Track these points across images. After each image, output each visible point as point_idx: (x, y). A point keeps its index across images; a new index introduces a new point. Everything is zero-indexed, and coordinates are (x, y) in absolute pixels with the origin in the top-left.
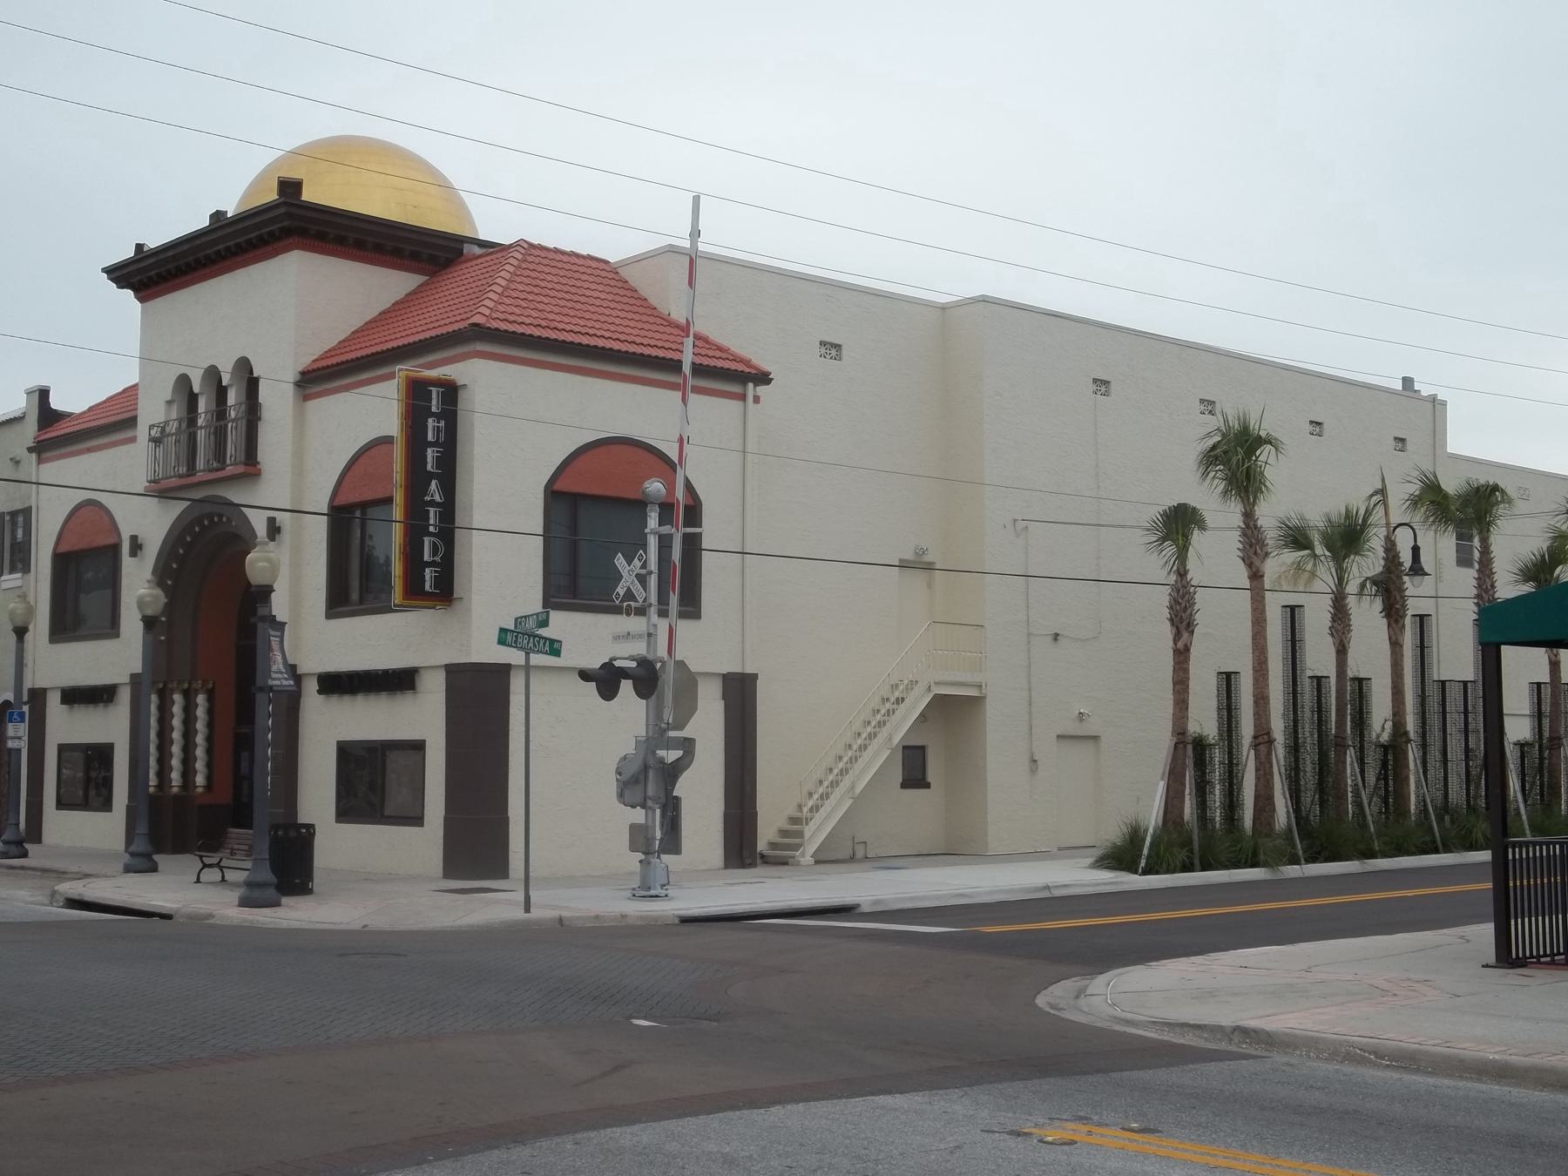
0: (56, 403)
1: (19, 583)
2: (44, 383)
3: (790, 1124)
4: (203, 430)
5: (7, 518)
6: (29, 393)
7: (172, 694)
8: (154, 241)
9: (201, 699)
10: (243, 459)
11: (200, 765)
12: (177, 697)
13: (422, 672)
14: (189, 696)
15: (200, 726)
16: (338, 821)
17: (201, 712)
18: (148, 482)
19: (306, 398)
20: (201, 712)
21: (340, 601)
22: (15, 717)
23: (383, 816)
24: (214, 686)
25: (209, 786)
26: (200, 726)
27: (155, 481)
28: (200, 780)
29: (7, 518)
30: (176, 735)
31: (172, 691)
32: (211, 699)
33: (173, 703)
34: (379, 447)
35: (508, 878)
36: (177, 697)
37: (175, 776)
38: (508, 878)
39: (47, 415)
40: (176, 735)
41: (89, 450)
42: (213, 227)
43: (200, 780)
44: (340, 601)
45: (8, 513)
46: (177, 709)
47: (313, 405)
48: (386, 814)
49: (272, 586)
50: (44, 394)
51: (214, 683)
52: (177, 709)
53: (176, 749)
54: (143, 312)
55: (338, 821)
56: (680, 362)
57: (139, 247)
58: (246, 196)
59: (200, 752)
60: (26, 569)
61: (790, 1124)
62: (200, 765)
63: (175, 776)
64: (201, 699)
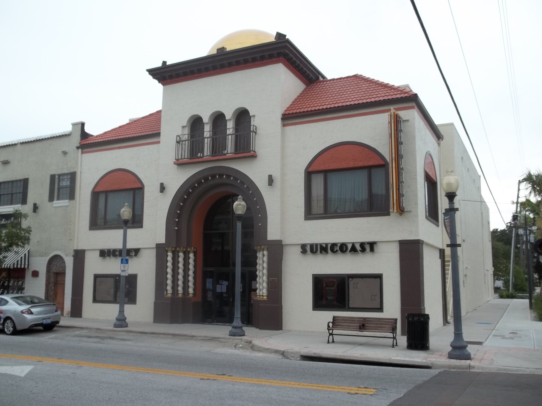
0: (87, 130)
1: (67, 204)
2: (83, 121)
3: (65, 388)
4: (187, 142)
5: (57, 177)
6: (74, 125)
7: (189, 254)
8: (170, 62)
9: (191, 255)
10: (234, 152)
11: (191, 284)
12: (181, 255)
13: (378, 243)
14: (186, 254)
15: (191, 267)
16: (314, 309)
17: (191, 261)
18: (176, 160)
19: (284, 125)
20: (191, 261)
21: (94, 225)
22: (124, 261)
23: (349, 308)
24: (196, 250)
25: (195, 294)
26: (191, 267)
27: (177, 160)
28: (191, 291)
29: (57, 177)
30: (181, 271)
31: (178, 252)
32: (195, 256)
33: (179, 257)
34: (343, 146)
35: (281, 329)
36: (181, 255)
37: (180, 289)
38: (281, 329)
39: (84, 135)
40: (181, 271)
41: (120, 148)
42: (163, 67)
43: (191, 291)
44: (94, 225)
45: (58, 175)
46: (181, 259)
47: (288, 128)
48: (350, 306)
49: (455, 193)
50: (83, 125)
51: (197, 249)
52: (181, 259)
53: (180, 277)
54: (164, 90)
55: (314, 309)
56: (237, 151)
57: (164, 63)
58: (210, 52)
59: (191, 278)
60: (72, 196)
61: (65, 388)
62: (191, 284)
63: (180, 289)
64: (191, 255)
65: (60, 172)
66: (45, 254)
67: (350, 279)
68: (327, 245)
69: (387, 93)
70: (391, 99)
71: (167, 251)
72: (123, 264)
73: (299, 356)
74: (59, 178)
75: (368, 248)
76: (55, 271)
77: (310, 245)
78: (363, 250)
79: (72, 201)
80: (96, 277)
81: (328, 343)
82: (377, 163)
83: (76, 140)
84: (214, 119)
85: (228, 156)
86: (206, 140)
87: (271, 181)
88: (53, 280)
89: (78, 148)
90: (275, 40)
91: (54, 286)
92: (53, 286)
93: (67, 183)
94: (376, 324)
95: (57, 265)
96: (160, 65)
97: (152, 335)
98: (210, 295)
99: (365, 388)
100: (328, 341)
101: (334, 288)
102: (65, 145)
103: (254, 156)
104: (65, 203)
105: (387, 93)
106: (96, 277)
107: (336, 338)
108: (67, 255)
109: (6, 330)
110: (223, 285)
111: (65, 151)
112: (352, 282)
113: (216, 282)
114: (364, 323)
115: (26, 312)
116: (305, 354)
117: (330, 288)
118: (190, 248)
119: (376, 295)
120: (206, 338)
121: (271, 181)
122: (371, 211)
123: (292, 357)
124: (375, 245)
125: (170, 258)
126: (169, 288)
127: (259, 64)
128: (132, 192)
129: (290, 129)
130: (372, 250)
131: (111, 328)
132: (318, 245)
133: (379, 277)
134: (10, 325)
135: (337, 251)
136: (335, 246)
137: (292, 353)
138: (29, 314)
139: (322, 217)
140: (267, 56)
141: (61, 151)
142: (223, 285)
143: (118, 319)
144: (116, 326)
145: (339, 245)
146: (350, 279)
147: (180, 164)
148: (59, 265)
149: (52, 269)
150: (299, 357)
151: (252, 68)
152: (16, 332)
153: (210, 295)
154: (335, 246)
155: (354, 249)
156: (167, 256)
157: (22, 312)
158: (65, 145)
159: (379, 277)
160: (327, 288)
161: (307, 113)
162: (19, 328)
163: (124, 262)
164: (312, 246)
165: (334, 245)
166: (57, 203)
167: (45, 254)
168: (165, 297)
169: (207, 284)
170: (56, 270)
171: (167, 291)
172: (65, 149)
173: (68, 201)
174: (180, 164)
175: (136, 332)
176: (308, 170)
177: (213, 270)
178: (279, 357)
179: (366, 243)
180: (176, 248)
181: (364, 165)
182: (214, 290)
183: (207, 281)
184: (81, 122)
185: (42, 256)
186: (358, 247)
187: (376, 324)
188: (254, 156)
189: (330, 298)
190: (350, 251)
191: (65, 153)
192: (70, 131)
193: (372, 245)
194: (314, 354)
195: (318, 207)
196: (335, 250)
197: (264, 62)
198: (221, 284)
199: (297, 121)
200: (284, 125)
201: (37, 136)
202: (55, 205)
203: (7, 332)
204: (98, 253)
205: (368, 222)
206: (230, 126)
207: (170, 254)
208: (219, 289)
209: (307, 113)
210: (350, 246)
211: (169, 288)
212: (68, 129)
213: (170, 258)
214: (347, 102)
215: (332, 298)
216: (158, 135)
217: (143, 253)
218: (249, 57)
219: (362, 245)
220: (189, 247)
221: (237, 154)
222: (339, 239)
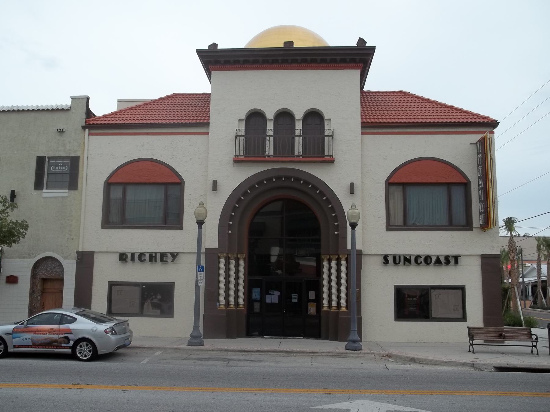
1: (66, 195)
5: (47, 160)
9: (242, 262)
12: (233, 261)
14: (237, 260)
16: (396, 320)
22: (200, 268)
36: (233, 261)
37: (232, 299)
39: (89, 114)
41: (148, 134)
46: (232, 267)
50: (88, 99)
52: (232, 267)
55: (396, 320)
57: (361, 41)
58: (251, 42)
65: (52, 154)
66: (29, 255)
67: (113, 287)
68: (156, 254)
69: (151, 117)
70: (133, 124)
71: (219, 258)
72: (200, 272)
73: (493, 368)
74: (49, 161)
75: (452, 261)
76: (44, 277)
77: (149, 254)
78: (448, 262)
79: (72, 192)
80: (112, 285)
81: (469, 351)
82: (459, 181)
83: (80, 118)
84: (247, 116)
85: (326, 158)
86: (297, 138)
87: (352, 189)
88: (39, 288)
89: (84, 128)
90: (357, 46)
91: (41, 296)
92: (39, 296)
93: (55, 169)
94: (512, 333)
95: (46, 270)
96: (353, 43)
97: (258, 353)
98: (257, 306)
99: (78, 384)
100: (470, 349)
101: (415, 298)
102: (60, 122)
103: (331, 161)
104: (63, 192)
105: (151, 117)
106: (112, 285)
107: (476, 348)
108: (65, 258)
109: (79, 355)
110: (273, 295)
111: (63, 130)
112: (434, 294)
113: (265, 292)
114: (500, 333)
115: (110, 331)
116: (498, 366)
117: (411, 299)
118: (242, 254)
119: (458, 306)
120: (330, 354)
121: (352, 189)
122: (165, 225)
123: (486, 368)
124: (459, 258)
125: (222, 265)
126: (222, 299)
127: (239, 67)
128: (163, 188)
129: (369, 138)
130: (456, 262)
131: (184, 346)
132: (401, 256)
133: (462, 289)
134: (86, 349)
135: (421, 262)
136: (143, 255)
137: (484, 365)
138: (112, 334)
139: (401, 229)
140: (328, 61)
141: (55, 129)
142: (273, 295)
143: (192, 336)
144: (190, 344)
145: (423, 257)
146: (432, 290)
147: (237, 161)
148: (51, 269)
149: (39, 275)
150: (493, 369)
151: (332, 69)
152: (96, 357)
153: (257, 306)
154: (143, 255)
155: (438, 262)
156: (219, 262)
157: (105, 331)
158: (60, 122)
159: (462, 289)
160: (409, 299)
161: (416, 124)
162: (101, 351)
163: (200, 270)
164: (395, 257)
165: (418, 257)
166: (47, 193)
167: (29, 255)
168: (218, 309)
169: (254, 294)
170: (45, 275)
171: (219, 301)
172: (61, 127)
173: (67, 191)
174: (237, 161)
175: (234, 351)
176: (108, 181)
177: (261, 278)
178: (472, 370)
179: (450, 256)
180: (228, 254)
181: (447, 182)
182: (262, 300)
183: (253, 291)
184: (86, 97)
185: (24, 258)
186: (442, 259)
187: (512, 333)
188: (331, 161)
189: (412, 309)
190: (435, 263)
191: (61, 132)
192: (67, 105)
193: (456, 258)
194: (508, 364)
195: (399, 220)
196: (143, 260)
197: (303, 66)
198: (271, 294)
199: (376, 131)
200: (362, 133)
201: (10, 106)
202: (44, 195)
203: (81, 358)
204: (117, 256)
205: (451, 236)
206: (298, 126)
207: (222, 261)
208: (268, 299)
209: (416, 124)
210: (434, 259)
211: (222, 299)
212: (67, 102)
213: (222, 265)
214: (151, 120)
215: (414, 308)
216: (207, 125)
217: (182, 259)
218: (338, 58)
219: (447, 258)
220: (230, 253)
221: (306, 157)
222: (423, 251)
